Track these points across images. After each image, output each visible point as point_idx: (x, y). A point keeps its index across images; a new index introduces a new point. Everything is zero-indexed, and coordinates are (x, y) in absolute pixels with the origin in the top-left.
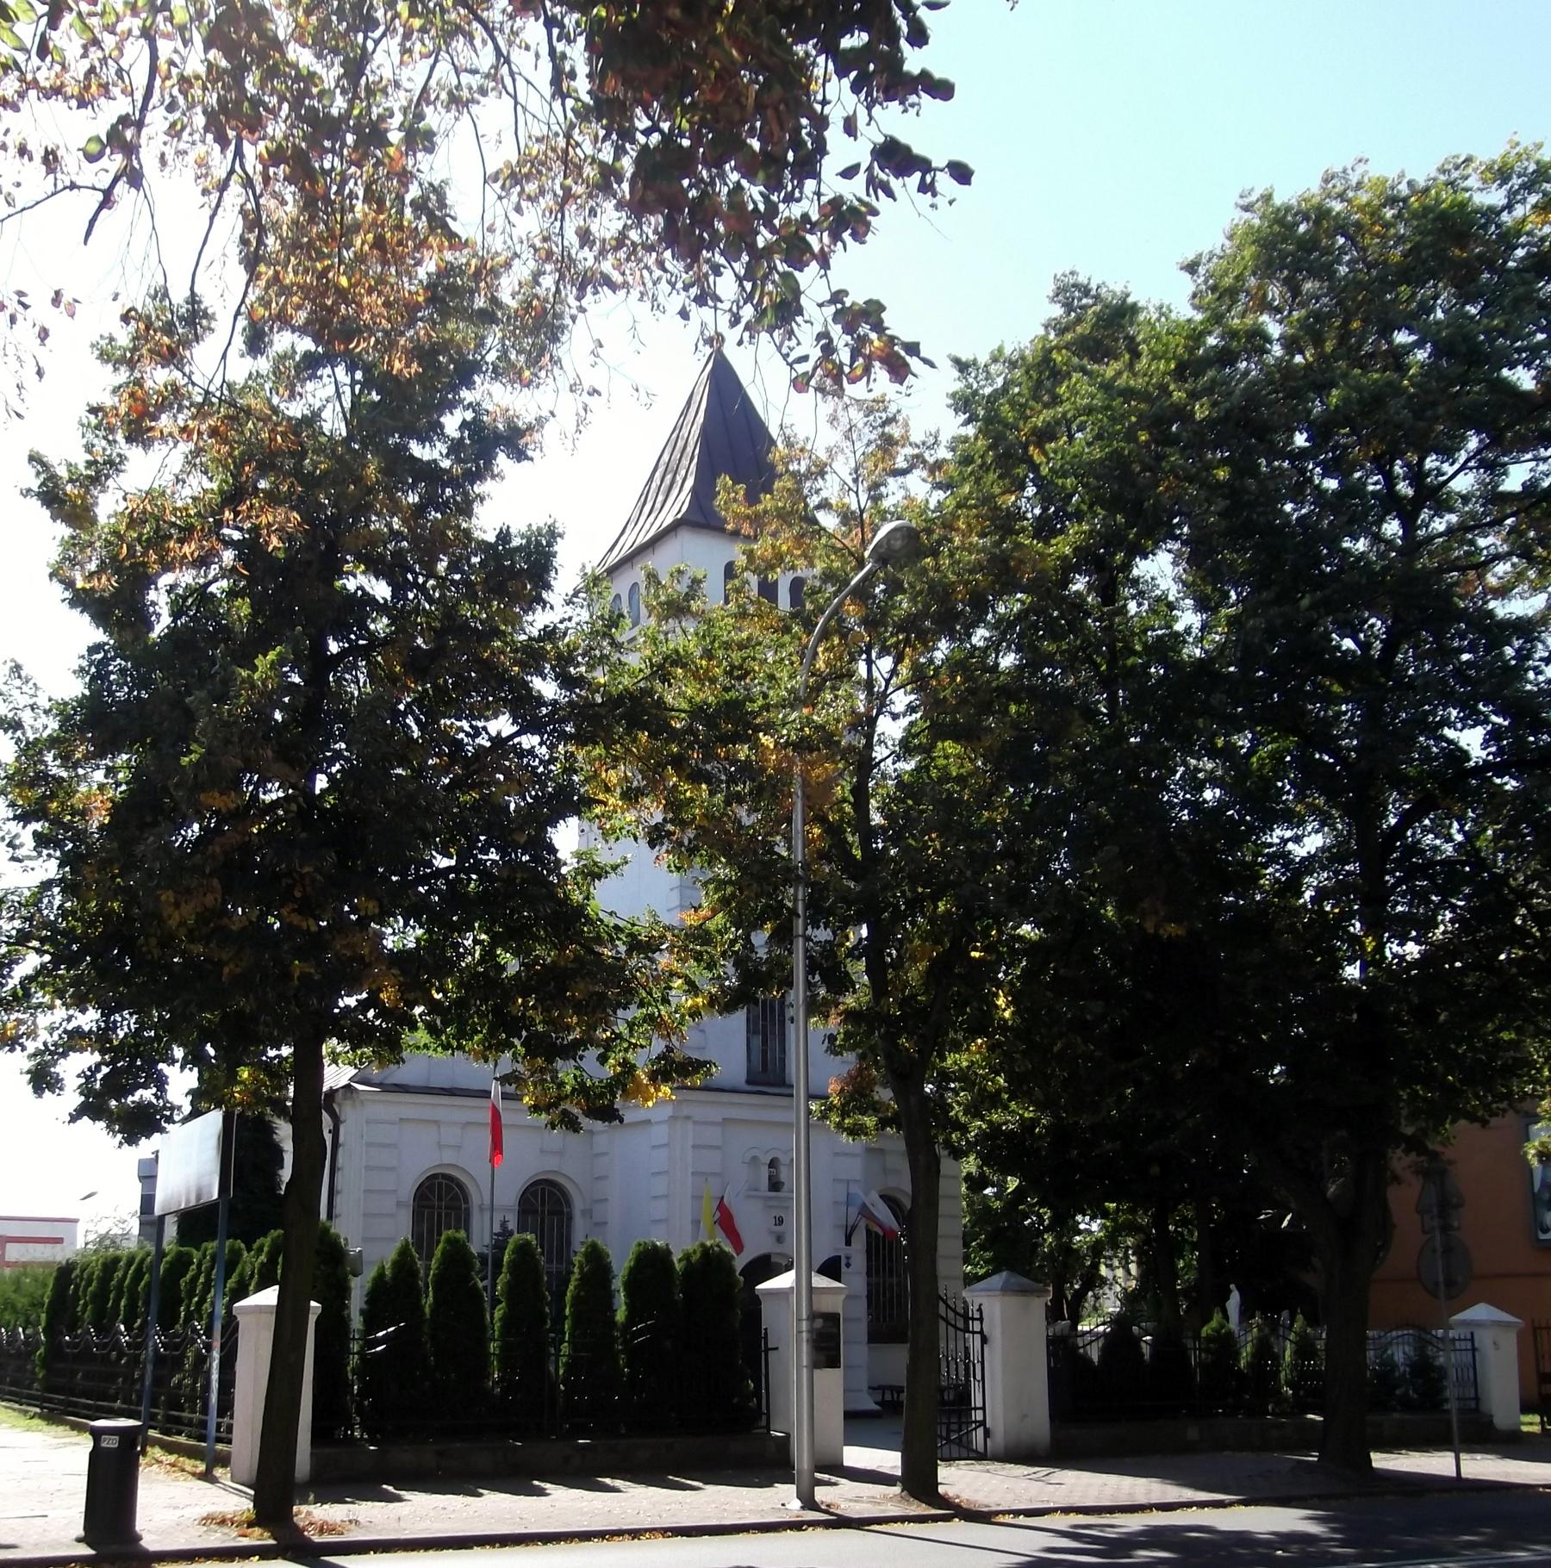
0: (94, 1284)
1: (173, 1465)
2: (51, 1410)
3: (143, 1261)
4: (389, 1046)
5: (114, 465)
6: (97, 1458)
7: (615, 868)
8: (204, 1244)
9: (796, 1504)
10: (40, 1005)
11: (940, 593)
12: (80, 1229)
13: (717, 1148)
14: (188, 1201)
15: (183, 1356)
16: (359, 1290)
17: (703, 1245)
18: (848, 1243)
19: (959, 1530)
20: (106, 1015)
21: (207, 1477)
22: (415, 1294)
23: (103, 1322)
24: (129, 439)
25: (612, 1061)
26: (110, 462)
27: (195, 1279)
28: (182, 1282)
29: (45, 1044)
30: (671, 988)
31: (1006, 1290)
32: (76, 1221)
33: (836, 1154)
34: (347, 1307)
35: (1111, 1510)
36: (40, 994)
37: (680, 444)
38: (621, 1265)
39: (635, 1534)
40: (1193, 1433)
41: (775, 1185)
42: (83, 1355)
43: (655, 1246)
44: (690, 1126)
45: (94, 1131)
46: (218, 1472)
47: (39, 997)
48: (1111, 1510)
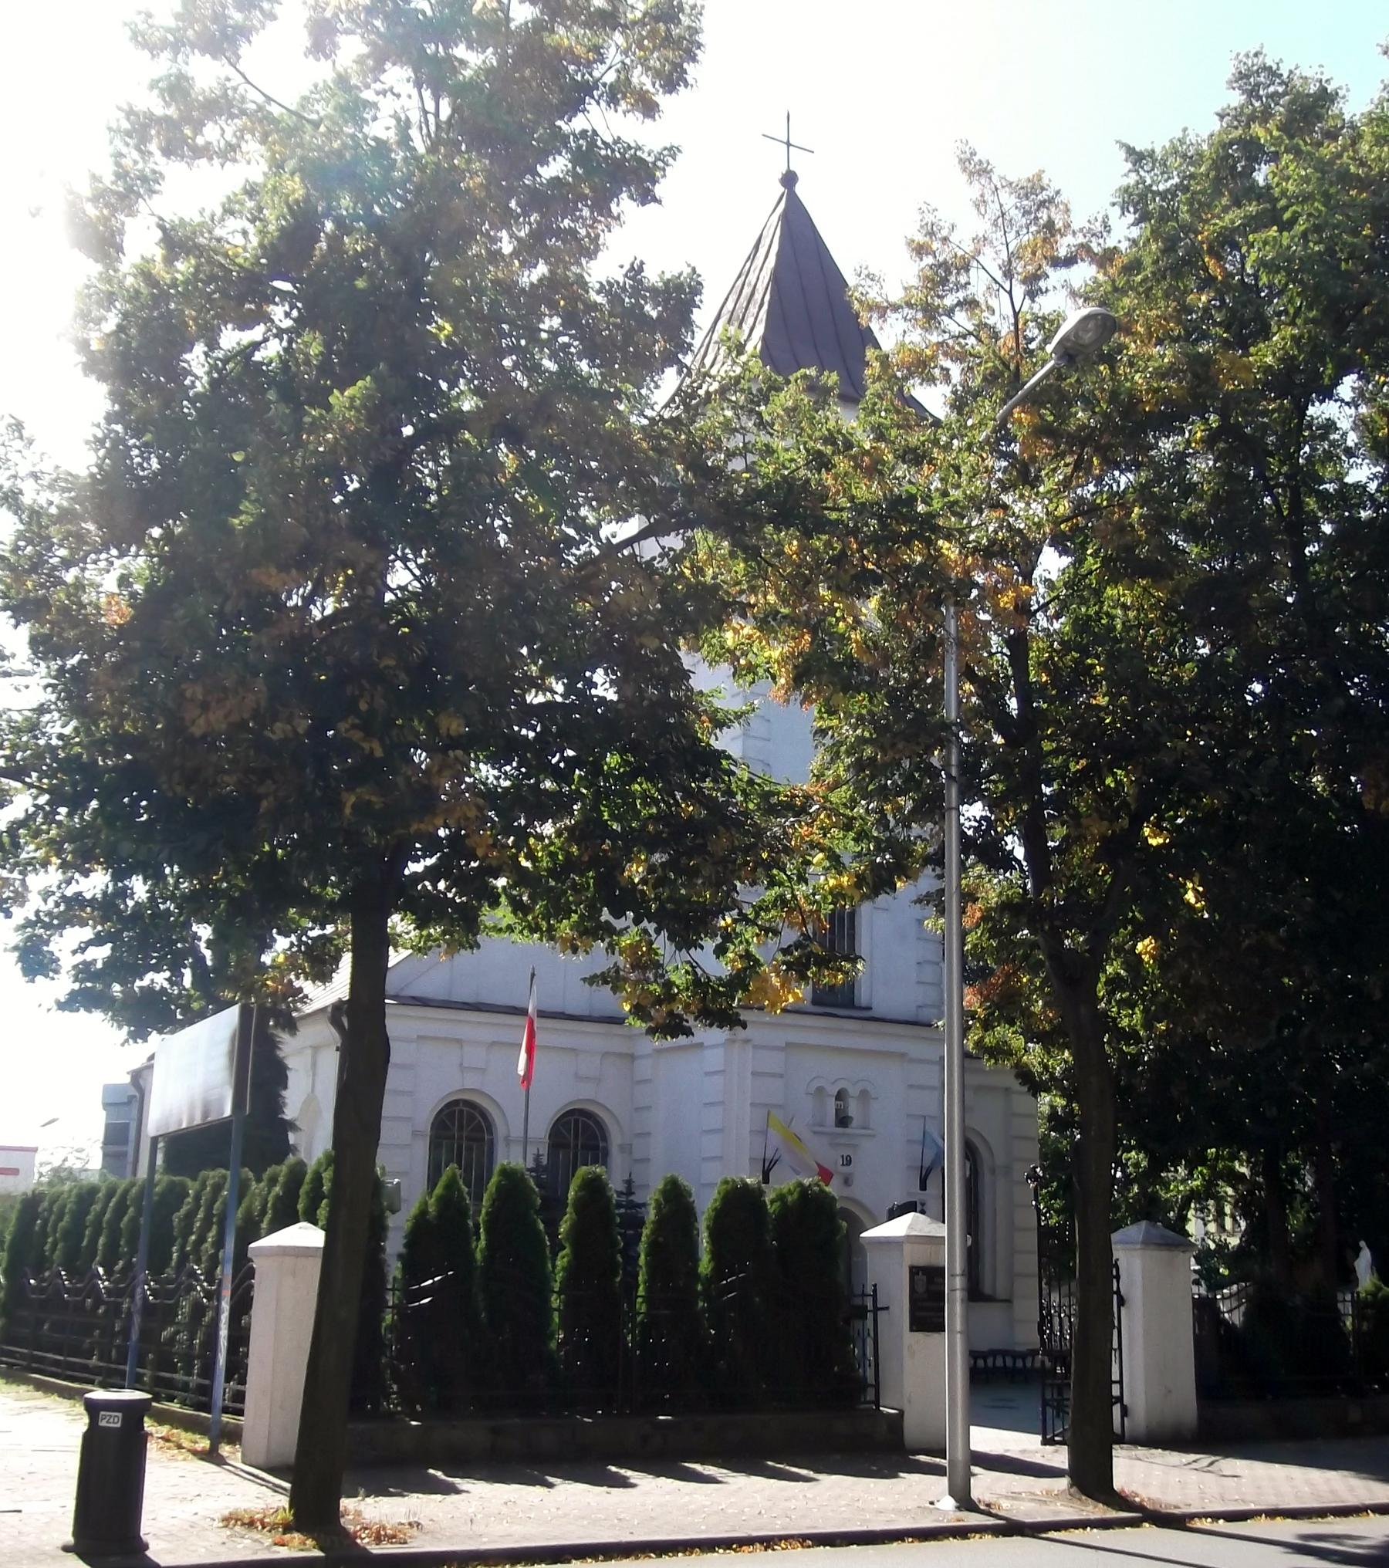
0: (66, 1218)
1: (166, 1439)
2: (10, 1365)
3: (126, 1192)
4: (464, 926)
5: (150, 182)
6: (93, 1444)
7: (738, 716)
8: (203, 1173)
9: (948, 1503)
10: (30, 862)
11: (1126, 404)
12: (39, 1158)
13: (781, 1076)
14: (191, 1117)
15: (177, 1305)
16: (398, 1227)
17: (800, 1184)
18: (923, 1187)
19: (1149, 1538)
20: (117, 877)
21: (211, 1456)
22: (465, 1236)
23: (77, 1262)
24: (167, 152)
25: (731, 955)
26: (144, 179)
27: (190, 1216)
28: (176, 1218)
29: (37, 913)
30: (809, 863)
31: (1147, 1243)
32: (35, 1150)
33: (911, 1086)
34: (383, 1250)
35: (1321, 1513)
36: (32, 847)
37: (747, 291)
38: (706, 1203)
39: (768, 1542)
40: (1355, 1414)
41: (843, 1120)
42: (52, 1301)
43: (745, 1185)
45: (96, 1023)
46: (225, 1450)
47: (30, 851)
48: (1321, 1513)
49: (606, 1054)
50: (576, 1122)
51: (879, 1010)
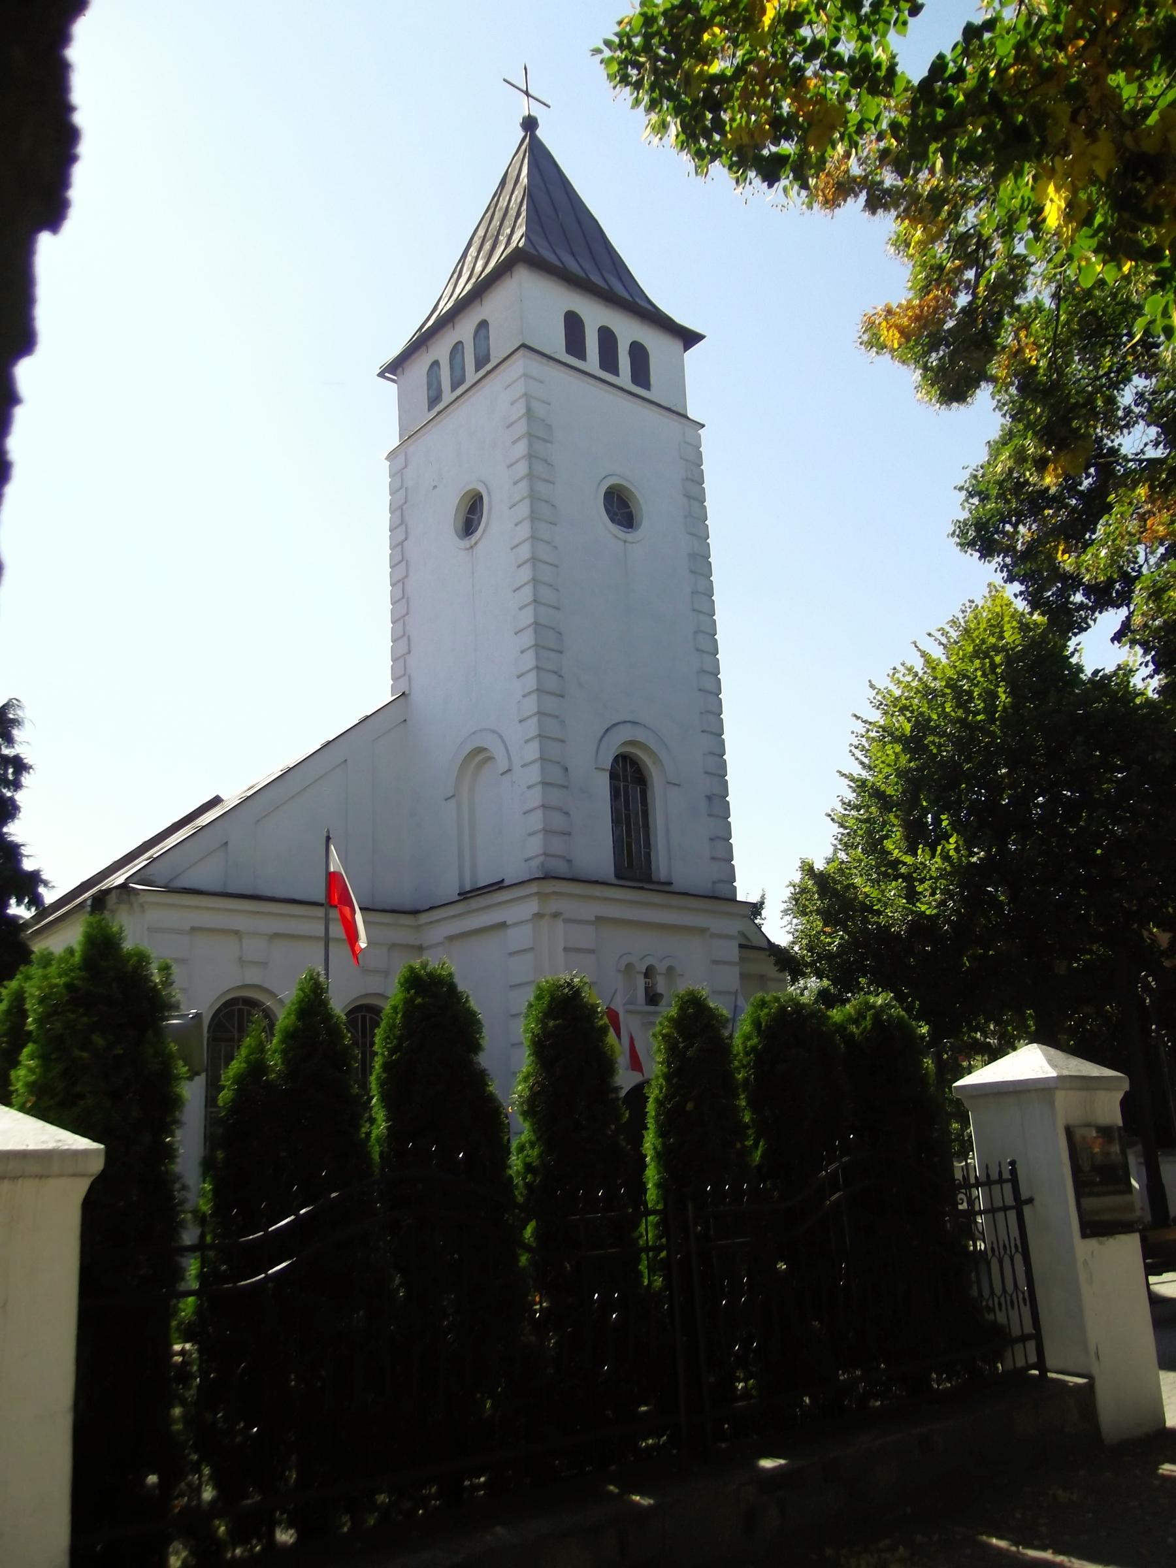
13: (592, 951)
33: (715, 962)
37: (487, 246)
44: (560, 925)
49: (394, 946)
50: (364, 1018)
51: (680, 884)
